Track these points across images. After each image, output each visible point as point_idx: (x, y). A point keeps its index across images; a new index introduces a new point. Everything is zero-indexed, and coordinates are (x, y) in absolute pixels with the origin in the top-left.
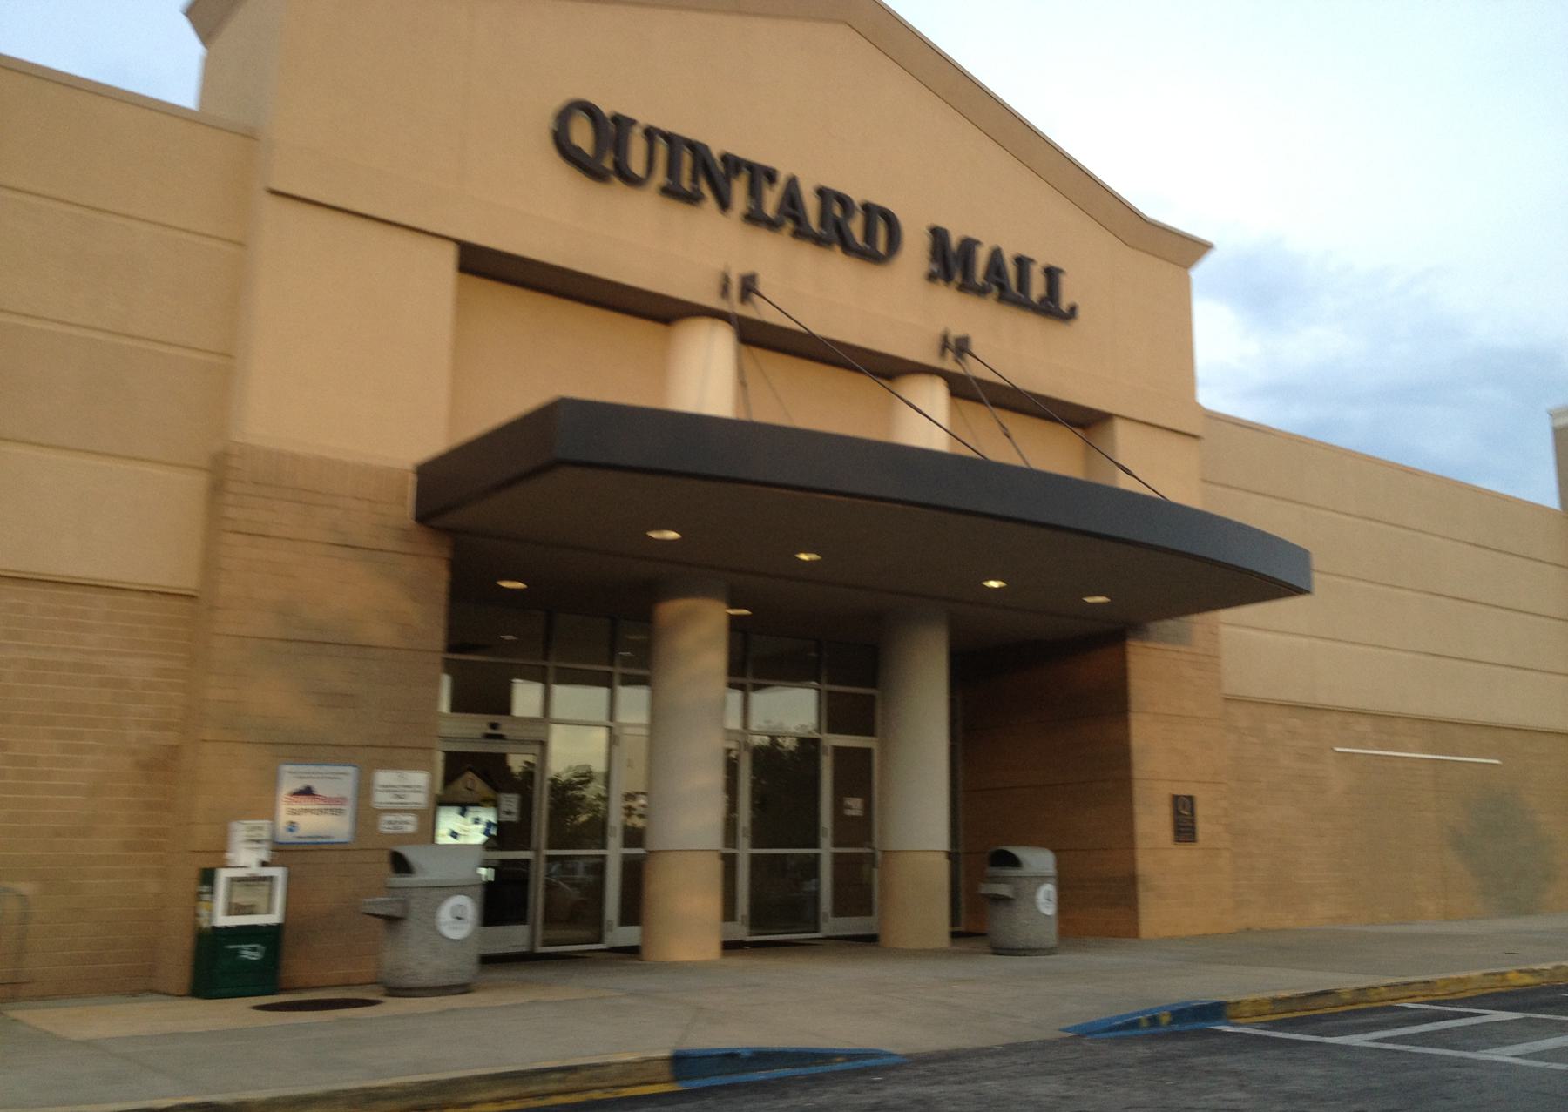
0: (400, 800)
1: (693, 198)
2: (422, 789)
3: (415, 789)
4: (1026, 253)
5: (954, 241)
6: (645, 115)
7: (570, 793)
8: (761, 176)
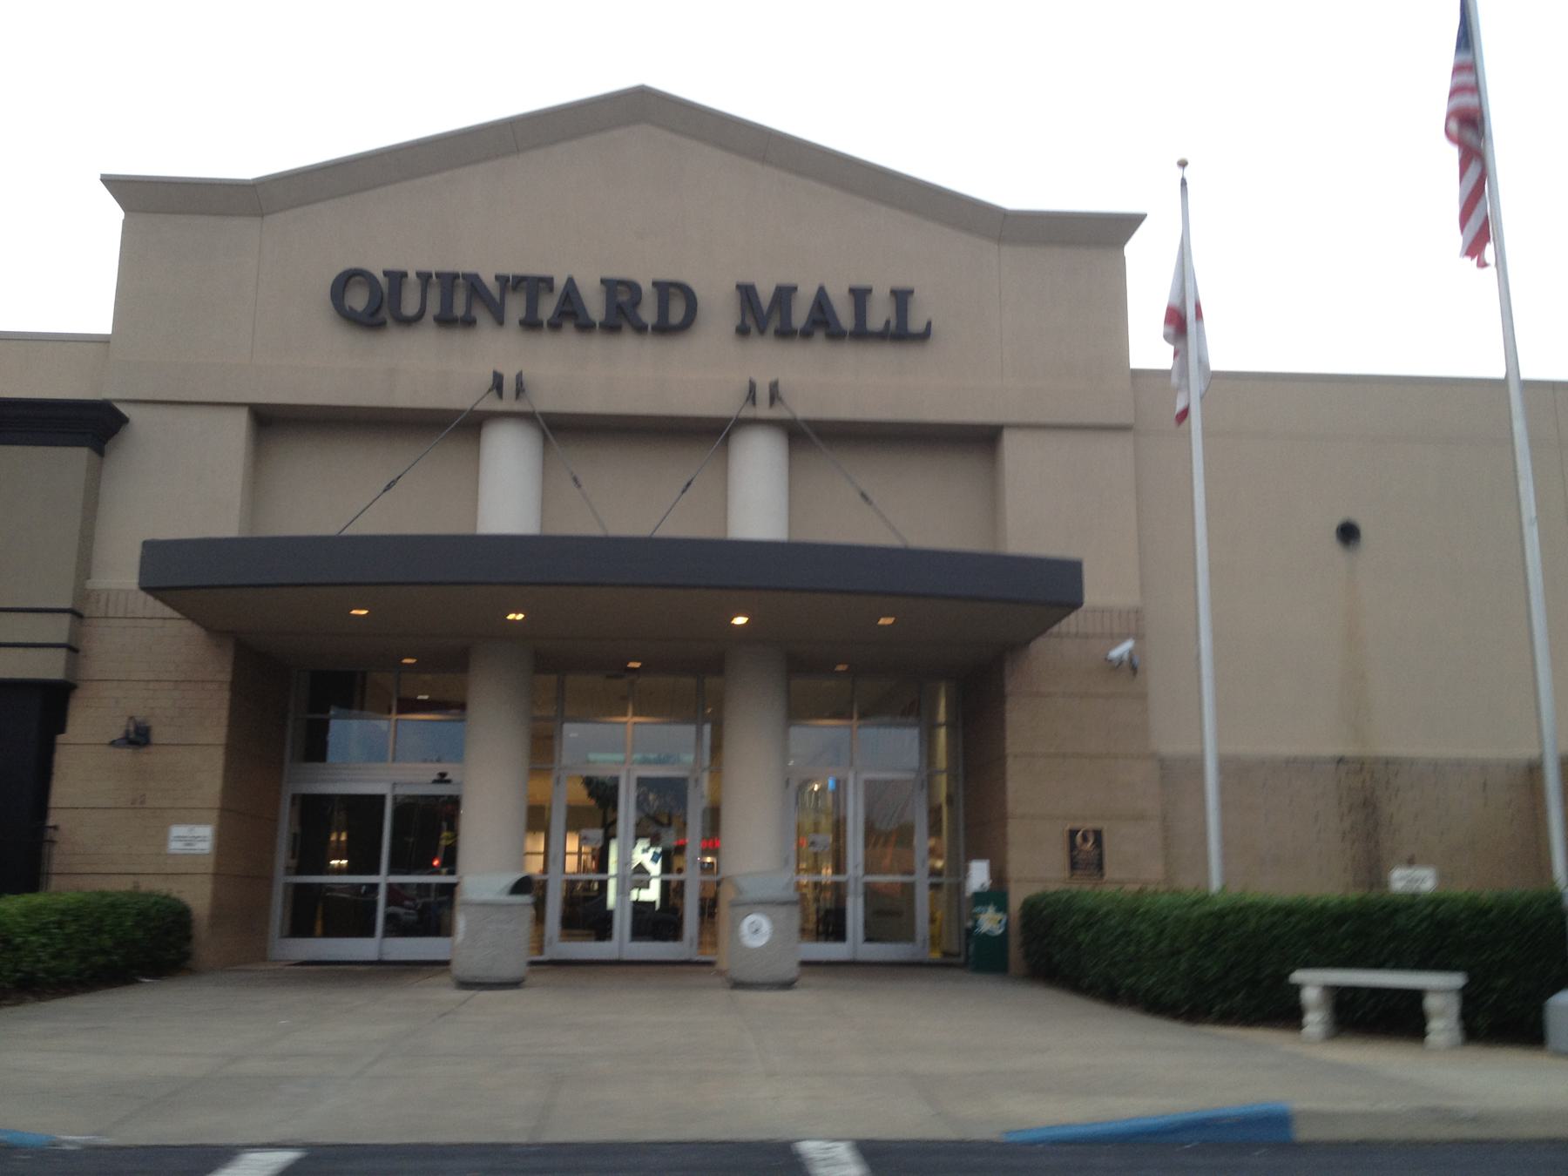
0: (189, 847)
1: (469, 322)
2: (823, 1163)
3: (203, 840)
4: (862, 282)
5: (765, 293)
6: (412, 265)
7: (1045, 913)
8: (534, 286)
